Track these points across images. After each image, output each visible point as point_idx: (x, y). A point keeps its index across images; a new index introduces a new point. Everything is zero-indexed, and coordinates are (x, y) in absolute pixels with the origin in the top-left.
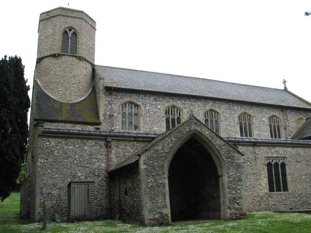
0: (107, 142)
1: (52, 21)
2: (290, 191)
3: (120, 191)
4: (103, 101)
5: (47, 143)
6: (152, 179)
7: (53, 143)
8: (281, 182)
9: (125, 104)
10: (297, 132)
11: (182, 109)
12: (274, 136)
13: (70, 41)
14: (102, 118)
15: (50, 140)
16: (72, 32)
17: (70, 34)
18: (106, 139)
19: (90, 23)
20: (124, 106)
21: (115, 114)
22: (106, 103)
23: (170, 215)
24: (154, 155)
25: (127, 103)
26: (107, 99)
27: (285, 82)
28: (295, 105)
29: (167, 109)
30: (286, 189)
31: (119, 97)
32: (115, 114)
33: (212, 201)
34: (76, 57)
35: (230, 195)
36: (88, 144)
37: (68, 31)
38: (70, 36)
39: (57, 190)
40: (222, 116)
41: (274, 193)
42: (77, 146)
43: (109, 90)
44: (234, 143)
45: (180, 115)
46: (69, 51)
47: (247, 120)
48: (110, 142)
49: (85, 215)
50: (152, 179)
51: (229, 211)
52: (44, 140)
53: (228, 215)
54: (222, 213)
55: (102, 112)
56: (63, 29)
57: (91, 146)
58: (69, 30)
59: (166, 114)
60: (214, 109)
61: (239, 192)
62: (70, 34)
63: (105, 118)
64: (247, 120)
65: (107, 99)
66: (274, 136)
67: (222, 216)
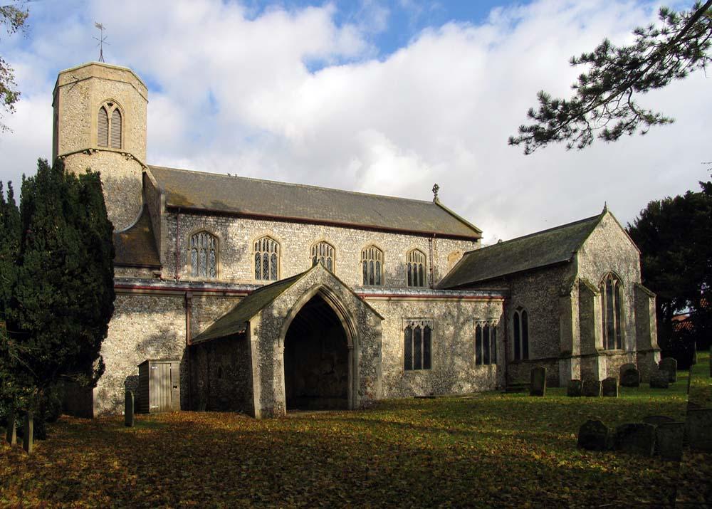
0: (186, 299)
1: (81, 88)
2: (434, 368)
3: (209, 371)
4: (166, 227)
8: (422, 356)
9: (196, 234)
10: (105, 206)
11: (280, 241)
12: (413, 282)
14: (163, 258)
16: (113, 108)
18: (186, 295)
20: (195, 237)
21: (182, 251)
22: (170, 233)
23: (285, 404)
24: (267, 322)
26: (170, 226)
27: (436, 189)
28: (466, 235)
29: (258, 242)
30: (427, 365)
31: (188, 224)
32: (182, 251)
33: (331, 384)
34: (121, 153)
37: (107, 107)
39: (121, 372)
40: (338, 252)
41: (411, 372)
42: (146, 306)
43: (174, 211)
45: (275, 251)
48: (190, 299)
49: (167, 406)
51: (359, 398)
54: (351, 401)
55: (163, 247)
58: (108, 104)
59: (256, 250)
60: (327, 240)
62: (111, 111)
63: (167, 258)
65: (170, 226)
66: (413, 282)
67: (351, 404)
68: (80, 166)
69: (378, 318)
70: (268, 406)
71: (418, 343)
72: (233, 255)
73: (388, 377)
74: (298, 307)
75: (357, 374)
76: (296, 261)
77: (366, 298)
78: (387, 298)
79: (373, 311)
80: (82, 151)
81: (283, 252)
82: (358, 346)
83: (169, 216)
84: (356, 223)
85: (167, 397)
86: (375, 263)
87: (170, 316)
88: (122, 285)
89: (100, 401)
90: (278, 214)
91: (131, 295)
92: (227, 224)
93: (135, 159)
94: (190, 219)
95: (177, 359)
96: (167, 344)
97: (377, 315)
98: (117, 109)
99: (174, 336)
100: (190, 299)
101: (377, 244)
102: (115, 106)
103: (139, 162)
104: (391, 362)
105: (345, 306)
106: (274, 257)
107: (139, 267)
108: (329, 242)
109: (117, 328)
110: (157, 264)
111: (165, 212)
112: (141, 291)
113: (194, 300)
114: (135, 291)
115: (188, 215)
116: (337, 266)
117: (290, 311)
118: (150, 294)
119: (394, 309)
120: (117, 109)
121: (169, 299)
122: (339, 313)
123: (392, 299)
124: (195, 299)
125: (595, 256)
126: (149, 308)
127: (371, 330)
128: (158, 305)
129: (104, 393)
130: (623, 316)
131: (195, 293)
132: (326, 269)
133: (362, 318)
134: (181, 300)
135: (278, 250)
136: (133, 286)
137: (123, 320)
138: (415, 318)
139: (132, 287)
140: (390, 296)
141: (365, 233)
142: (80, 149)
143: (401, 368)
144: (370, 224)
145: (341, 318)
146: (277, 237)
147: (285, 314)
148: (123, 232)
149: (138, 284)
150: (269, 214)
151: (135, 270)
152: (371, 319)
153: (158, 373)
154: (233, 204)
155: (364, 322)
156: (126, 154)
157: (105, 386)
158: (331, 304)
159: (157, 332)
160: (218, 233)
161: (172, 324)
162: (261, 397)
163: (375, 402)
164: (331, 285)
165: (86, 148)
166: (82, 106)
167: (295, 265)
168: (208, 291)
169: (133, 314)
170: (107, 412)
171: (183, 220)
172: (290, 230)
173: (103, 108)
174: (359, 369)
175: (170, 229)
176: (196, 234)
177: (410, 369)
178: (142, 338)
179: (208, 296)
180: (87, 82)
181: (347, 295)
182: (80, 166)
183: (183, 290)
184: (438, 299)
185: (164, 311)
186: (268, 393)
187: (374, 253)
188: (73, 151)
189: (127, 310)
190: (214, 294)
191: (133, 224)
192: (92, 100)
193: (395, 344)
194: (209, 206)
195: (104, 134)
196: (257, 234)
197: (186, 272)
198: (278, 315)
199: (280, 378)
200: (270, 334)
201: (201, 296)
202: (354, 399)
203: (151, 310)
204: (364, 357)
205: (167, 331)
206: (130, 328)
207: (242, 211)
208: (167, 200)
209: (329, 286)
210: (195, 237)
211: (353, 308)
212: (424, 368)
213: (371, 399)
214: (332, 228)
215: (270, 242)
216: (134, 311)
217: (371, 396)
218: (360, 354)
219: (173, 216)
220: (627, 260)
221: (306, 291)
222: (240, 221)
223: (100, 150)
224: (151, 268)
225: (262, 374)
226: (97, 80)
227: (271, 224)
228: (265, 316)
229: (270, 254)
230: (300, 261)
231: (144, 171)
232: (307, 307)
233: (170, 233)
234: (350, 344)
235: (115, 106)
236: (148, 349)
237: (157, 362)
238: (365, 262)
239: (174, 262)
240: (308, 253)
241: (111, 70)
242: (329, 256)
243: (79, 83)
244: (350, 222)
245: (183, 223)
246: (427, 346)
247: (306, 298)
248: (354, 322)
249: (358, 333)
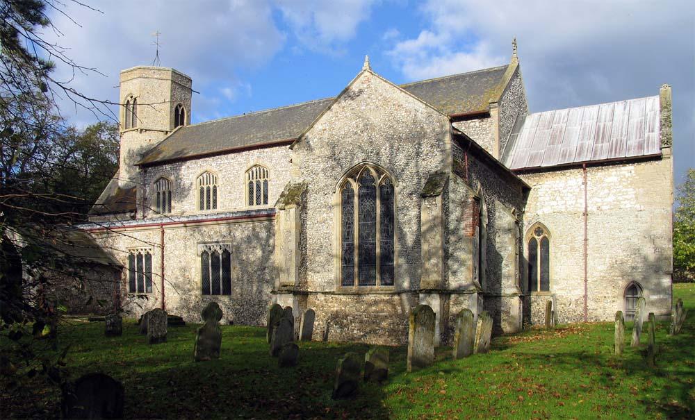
2: (233, 295)
12: (211, 205)
25: (160, 179)
41: (208, 296)
47: (205, 183)
71: (215, 268)
72: (183, 193)
76: (231, 189)
78: (182, 225)
93: (146, 130)
106: (266, 183)
123: (187, 225)
125: (333, 146)
130: (400, 217)
138: (212, 242)
143: (198, 292)
144: (465, 112)
146: (215, 170)
167: (230, 193)
177: (209, 293)
184: (240, 220)
212: (224, 294)
214: (266, 150)
220: (416, 138)
222: (188, 163)
238: (251, 183)
246: (227, 270)
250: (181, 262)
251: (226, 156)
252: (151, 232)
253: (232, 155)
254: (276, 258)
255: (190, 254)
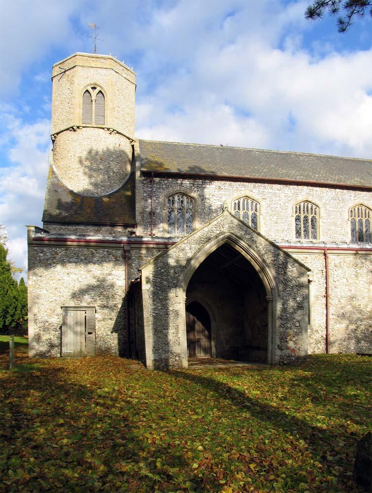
5: (42, 255)
6: (158, 305)
7: (48, 254)
13: (94, 106)
14: (138, 218)
15: (45, 249)
16: (97, 91)
17: (94, 93)
19: (124, 75)
22: (145, 195)
24: (163, 271)
34: (103, 129)
35: (282, 330)
36: (98, 255)
37: (90, 90)
38: (94, 98)
39: (56, 317)
40: (322, 211)
42: (83, 258)
43: (148, 175)
44: (323, 251)
46: (93, 121)
47: (364, 216)
48: (129, 251)
50: (158, 305)
51: (278, 352)
52: (35, 250)
53: (277, 358)
54: (269, 355)
55: (138, 206)
56: (82, 87)
57: (102, 257)
58: (92, 88)
61: (297, 324)
62: (94, 93)
63: (143, 217)
64: (364, 216)
65: (145, 189)
67: (269, 359)
68: (67, 142)
69: (303, 269)
70: (163, 356)
73: (355, 330)
74: (202, 258)
75: (276, 327)
77: (329, 251)
78: (354, 252)
79: (296, 261)
80: (68, 129)
81: (263, 211)
82: (277, 298)
83: (144, 180)
84: (341, 183)
85: (81, 343)
86: (364, 220)
87: (108, 267)
88: (57, 238)
89: (35, 344)
90: (257, 176)
91: (67, 247)
92: (204, 186)
93: (118, 133)
94: (166, 182)
95: (111, 308)
96: (105, 293)
97: (302, 265)
98: (100, 92)
99: (112, 286)
100: (129, 251)
101: (365, 203)
102: (98, 89)
103: (124, 136)
104: (359, 316)
105: (259, 256)
107: (113, 225)
108: (313, 201)
109: (53, 278)
110: (131, 222)
111: (140, 177)
112: (75, 243)
113: (133, 252)
114: (69, 243)
115: (163, 179)
116: (321, 224)
117: (189, 261)
118: (88, 247)
119: (362, 263)
120: (100, 92)
121: (107, 252)
122: (253, 263)
123: (360, 252)
124: (134, 251)
126: (86, 259)
127: (294, 282)
128: (95, 257)
129: (39, 337)
131: (133, 246)
132: (235, 217)
133: (281, 268)
134: (119, 253)
135: (258, 209)
136: (66, 239)
137: (59, 270)
139: (66, 240)
140: (357, 250)
141: (352, 193)
142: (67, 127)
144: (358, 184)
145: (257, 268)
147: (184, 263)
148: (105, 196)
149: (73, 237)
150: (248, 176)
151: (109, 228)
152: (292, 271)
153: (72, 319)
154: (208, 168)
155: (285, 273)
156: (108, 129)
157: (40, 330)
158: (244, 253)
159: (94, 282)
160: (194, 195)
161: (110, 274)
162: (154, 347)
163: (298, 358)
164: (240, 233)
165: (71, 126)
166: (69, 91)
167: (276, 223)
168: (147, 243)
169: (69, 266)
170: (42, 355)
171: (159, 183)
172: (271, 191)
173: (87, 91)
174: (278, 323)
175: (145, 192)
176: (173, 196)
178: (77, 287)
179: (148, 249)
180: (72, 71)
181: (261, 243)
182: (67, 142)
183: (120, 242)
185: (100, 262)
186: (162, 343)
187: (364, 211)
188: (63, 129)
189: (62, 260)
190: (155, 246)
191: (117, 189)
192: (76, 85)
193: (364, 298)
194: (185, 169)
195: (87, 112)
196: (236, 195)
197: (161, 229)
198: (175, 264)
199: (177, 328)
200: (165, 283)
201: (140, 249)
202: (273, 354)
203: (87, 261)
204: (284, 310)
205: (104, 280)
206: (66, 278)
207: (219, 174)
208: (142, 166)
209: (238, 234)
210: (171, 198)
211: (269, 258)
213: (293, 354)
215: (250, 201)
216: (71, 262)
217: (293, 350)
218: (279, 306)
219: (149, 180)
221: (209, 240)
222: (216, 184)
223: (83, 127)
224: (126, 226)
225: (155, 324)
226: (80, 68)
227: (251, 185)
228: (160, 264)
229: (250, 213)
230: (282, 219)
231: (132, 144)
232: (212, 258)
233: (145, 195)
234: (269, 297)
235: (98, 89)
236: (85, 297)
237: (70, 309)
239: (150, 220)
240: (346, 215)
241: (94, 59)
242: (367, 218)
243: (67, 72)
244: (335, 183)
245: (158, 186)
247: (212, 247)
248: (271, 273)
249: (277, 284)
250: (351, 291)
251: (270, 185)
252: (308, 256)
253: (278, 186)
254: (180, 291)
255: (362, 282)
